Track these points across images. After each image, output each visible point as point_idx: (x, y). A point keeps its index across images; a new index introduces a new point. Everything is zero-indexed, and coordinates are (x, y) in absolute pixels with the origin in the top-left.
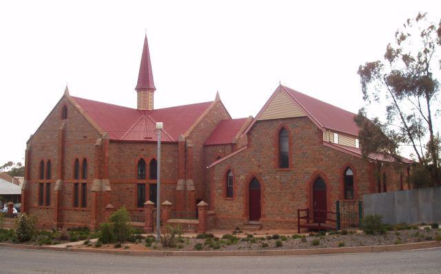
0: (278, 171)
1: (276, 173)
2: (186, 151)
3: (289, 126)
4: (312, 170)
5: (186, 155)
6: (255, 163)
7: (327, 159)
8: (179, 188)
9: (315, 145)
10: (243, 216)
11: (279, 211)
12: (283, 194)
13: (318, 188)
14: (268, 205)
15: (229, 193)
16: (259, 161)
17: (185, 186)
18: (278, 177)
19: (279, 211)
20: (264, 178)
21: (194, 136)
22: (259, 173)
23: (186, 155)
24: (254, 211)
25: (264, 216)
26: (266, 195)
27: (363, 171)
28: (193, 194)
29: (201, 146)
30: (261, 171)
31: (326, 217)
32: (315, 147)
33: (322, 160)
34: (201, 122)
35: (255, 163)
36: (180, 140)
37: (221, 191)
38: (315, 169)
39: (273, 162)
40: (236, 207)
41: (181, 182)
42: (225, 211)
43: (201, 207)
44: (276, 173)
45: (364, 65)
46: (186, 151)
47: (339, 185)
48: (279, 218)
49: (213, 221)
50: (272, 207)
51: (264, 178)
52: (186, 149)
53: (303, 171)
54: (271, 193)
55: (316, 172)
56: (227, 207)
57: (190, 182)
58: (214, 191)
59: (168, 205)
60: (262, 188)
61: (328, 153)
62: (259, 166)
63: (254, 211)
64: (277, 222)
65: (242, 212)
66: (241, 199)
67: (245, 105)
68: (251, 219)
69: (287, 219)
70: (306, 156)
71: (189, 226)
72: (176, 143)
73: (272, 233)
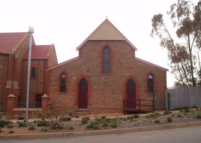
0: (102, 74)
1: (101, 76)
2: (14, 61)
3: (111, 45)
4: (127, 74)
5: (14, 64)
6: (85, 68)
7: (137, 68)
8: (8, 87)
9: (129, 59)
10: (74, 105)
11: (103, 101)
12: (105, 90)
13: (131, 87)
14: (94, 98)
15: (63, 89)
16: (88, 67)
17: (12, 86)
18: (102, 79)
19: (103, 101)
20: (91, 79)
21: (18, 52)
22: (88, 76)
23: (14, 64)
24: (83, 101)
25: (91, 105)
26: (93, 91)
27: (160, 76)
28: (18, 91)
29: (21, 60)
30: (89, 74)
31: (135, 104)
32: (129, 60)
33: (134, 68)
34: (22, 43)
35: (85, 68)
36: (10, 53)
37: (56, 87)
38: (129, 74)
39: (98, 69)
40: (69, 99)
41: (9, 82)
42: (59, 102)
43: (45, 98)
44: (101, 76)
45: (39, 40)
46: (14, 61)
47: (145, 84)
48: (102, 106)
49: (53, 109)
50: (97, 99)
51: (91, 79)
52: (14, 60)
53: (121, 76)
54: (97, 89)
55: (130, 76)
56: (61, 99)
57: (16, 83)
58: (51, 88)
59: (14, 98)
60: (89, 86)
61: (138, 64)
62: (88, 71)
63: (83, 101)
64: (101, 109)
65: (73, 103)
66: (73, 93)
67: (158, 14)
68: (79, 108)
69: (108, 106)
70: (123, 65)
71: (33, 113)
72: (7, 55)
73: (100, 116)
